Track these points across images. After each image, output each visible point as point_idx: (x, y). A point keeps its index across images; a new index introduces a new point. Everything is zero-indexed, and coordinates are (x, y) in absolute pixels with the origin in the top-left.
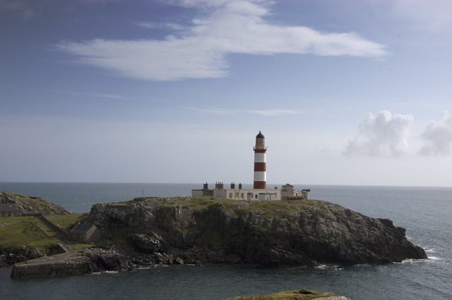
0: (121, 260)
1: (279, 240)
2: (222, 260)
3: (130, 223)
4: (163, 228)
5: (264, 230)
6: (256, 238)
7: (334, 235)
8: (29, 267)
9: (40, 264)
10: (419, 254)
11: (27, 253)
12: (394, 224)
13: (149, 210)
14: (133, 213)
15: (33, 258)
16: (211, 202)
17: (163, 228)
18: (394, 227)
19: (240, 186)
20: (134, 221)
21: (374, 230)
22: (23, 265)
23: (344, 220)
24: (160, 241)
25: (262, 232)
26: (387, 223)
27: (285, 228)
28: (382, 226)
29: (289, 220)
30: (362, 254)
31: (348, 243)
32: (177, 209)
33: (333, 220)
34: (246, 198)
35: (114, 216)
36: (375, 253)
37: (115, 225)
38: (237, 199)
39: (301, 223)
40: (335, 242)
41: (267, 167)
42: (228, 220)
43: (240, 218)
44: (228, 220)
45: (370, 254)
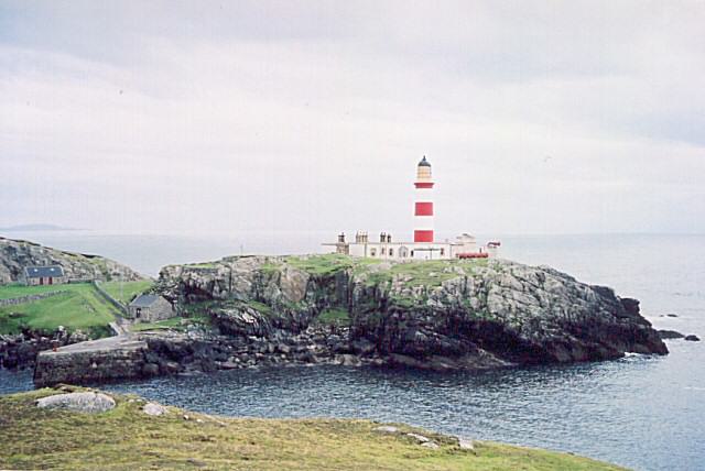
0: (193, 348)
1: (428, 318)
2: (347, 346)
3: (214, 294)
4: (264, 301)
5: (408, 303)
6: (395, 315)
7: (514, 311)
8: (58, 356)
9: (74, 352)
10: (649, 342)
11: (64, 336)
12: (616, 295)
13: (243, 275)
14: (219, 278)
15: (72, 343)
16: (338, 263)
17: (264, 301)
18: (615, 298)
19: (28, 104)
20: (221, 291)
21: (580, 303)
22: (49, 353)
23: (532, 288)
24: (258, 319)
25: (403, 307)
26: (606, 293)
27: (96, 272)
28: (595, 297)
29: (446, 289)
30: (555, 339)
31: (535, 322)
32: (283, 273)
33: (515, 289)
34: (395, 256)
35: (191, 283)
36: (576, 337)
37: (194, 296)
38: (383, 257)
39: (465, 292)
40: (515, 320)
41: (434, 209)
42: (357, 292)
43: (376, 285)
44: (357, 292)
45: (567, 338)
